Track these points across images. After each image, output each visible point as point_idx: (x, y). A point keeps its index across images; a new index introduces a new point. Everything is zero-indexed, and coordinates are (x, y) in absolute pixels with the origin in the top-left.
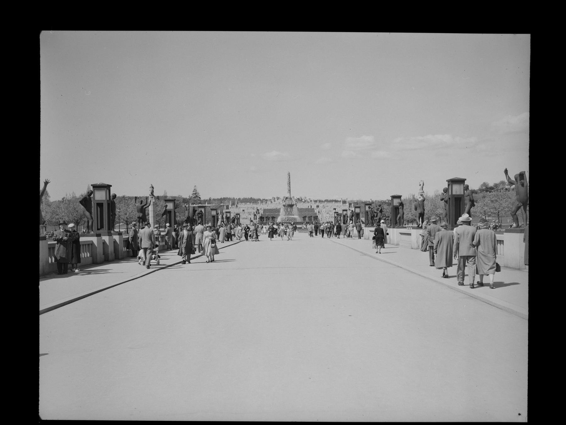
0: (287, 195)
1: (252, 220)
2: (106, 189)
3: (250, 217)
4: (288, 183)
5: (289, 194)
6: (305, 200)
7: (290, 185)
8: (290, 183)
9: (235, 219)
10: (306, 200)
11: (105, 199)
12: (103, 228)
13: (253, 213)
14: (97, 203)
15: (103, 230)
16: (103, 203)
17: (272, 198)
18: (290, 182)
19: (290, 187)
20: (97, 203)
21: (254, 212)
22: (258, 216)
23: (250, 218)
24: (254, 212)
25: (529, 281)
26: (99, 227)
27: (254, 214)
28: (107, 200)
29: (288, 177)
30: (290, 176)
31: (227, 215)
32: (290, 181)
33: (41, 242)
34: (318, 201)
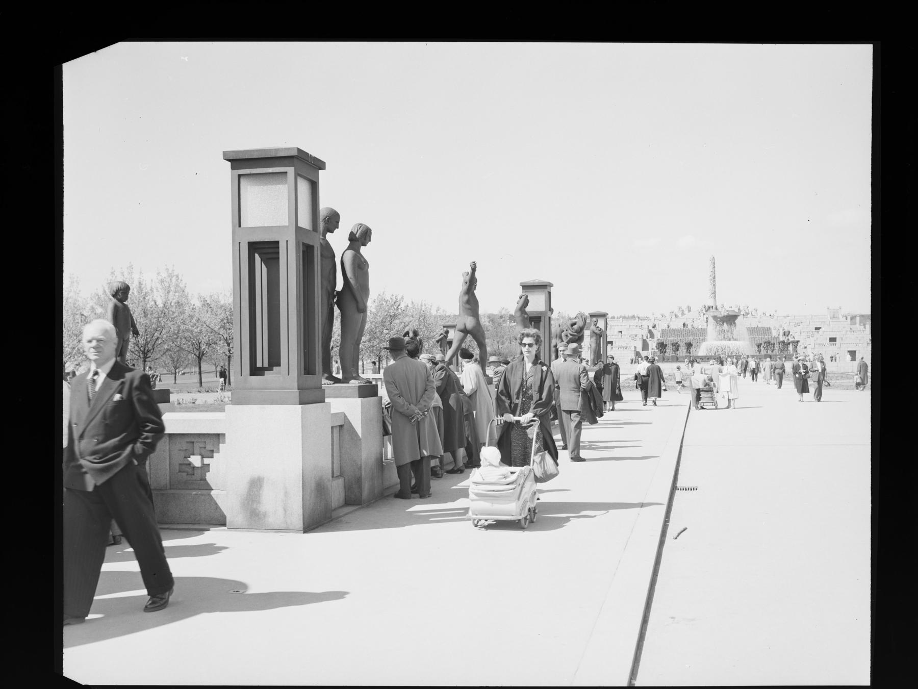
0: (710, 303)
1: (639, 352)
2: (291, 171)
3: (632, 344)
4: (711, 278)
5: (712, 300)
6: (746, 313)
7: (714, 281)
8: (714, 278)
9: (581, 330)
10: (747, 311)
11: (287, 224)
12: (279, 365)
13: (641, 337)
14: (249, 243)
15: (279, 373)
16: (277, 243)
17: (227, 407)
18: (715, 277)
19: (714, 285)
20: (249, 243)
21: (642, 336)
22: (653, 344)
23: (635, 347)
24: (642, 336)
25: (872, 485)
26: (262, 360)
27: (643, 338)
28: (299, 229)
29: (712, 266)
30: (714, 263)
31: (526, 302)
32: (714, 274)
33: (171, 395)
34: (858, 319)
